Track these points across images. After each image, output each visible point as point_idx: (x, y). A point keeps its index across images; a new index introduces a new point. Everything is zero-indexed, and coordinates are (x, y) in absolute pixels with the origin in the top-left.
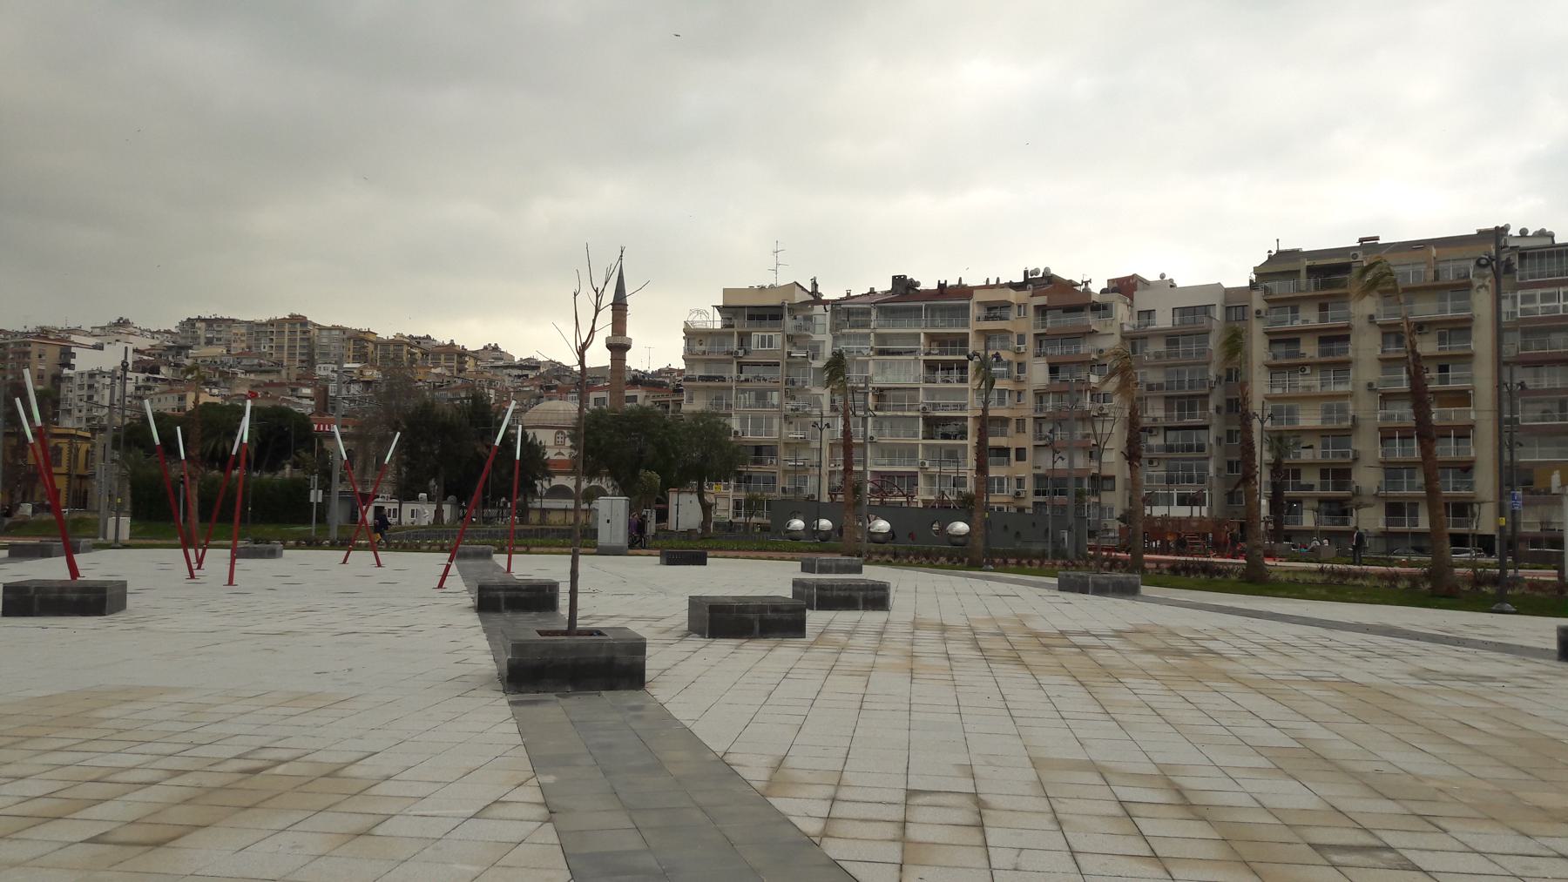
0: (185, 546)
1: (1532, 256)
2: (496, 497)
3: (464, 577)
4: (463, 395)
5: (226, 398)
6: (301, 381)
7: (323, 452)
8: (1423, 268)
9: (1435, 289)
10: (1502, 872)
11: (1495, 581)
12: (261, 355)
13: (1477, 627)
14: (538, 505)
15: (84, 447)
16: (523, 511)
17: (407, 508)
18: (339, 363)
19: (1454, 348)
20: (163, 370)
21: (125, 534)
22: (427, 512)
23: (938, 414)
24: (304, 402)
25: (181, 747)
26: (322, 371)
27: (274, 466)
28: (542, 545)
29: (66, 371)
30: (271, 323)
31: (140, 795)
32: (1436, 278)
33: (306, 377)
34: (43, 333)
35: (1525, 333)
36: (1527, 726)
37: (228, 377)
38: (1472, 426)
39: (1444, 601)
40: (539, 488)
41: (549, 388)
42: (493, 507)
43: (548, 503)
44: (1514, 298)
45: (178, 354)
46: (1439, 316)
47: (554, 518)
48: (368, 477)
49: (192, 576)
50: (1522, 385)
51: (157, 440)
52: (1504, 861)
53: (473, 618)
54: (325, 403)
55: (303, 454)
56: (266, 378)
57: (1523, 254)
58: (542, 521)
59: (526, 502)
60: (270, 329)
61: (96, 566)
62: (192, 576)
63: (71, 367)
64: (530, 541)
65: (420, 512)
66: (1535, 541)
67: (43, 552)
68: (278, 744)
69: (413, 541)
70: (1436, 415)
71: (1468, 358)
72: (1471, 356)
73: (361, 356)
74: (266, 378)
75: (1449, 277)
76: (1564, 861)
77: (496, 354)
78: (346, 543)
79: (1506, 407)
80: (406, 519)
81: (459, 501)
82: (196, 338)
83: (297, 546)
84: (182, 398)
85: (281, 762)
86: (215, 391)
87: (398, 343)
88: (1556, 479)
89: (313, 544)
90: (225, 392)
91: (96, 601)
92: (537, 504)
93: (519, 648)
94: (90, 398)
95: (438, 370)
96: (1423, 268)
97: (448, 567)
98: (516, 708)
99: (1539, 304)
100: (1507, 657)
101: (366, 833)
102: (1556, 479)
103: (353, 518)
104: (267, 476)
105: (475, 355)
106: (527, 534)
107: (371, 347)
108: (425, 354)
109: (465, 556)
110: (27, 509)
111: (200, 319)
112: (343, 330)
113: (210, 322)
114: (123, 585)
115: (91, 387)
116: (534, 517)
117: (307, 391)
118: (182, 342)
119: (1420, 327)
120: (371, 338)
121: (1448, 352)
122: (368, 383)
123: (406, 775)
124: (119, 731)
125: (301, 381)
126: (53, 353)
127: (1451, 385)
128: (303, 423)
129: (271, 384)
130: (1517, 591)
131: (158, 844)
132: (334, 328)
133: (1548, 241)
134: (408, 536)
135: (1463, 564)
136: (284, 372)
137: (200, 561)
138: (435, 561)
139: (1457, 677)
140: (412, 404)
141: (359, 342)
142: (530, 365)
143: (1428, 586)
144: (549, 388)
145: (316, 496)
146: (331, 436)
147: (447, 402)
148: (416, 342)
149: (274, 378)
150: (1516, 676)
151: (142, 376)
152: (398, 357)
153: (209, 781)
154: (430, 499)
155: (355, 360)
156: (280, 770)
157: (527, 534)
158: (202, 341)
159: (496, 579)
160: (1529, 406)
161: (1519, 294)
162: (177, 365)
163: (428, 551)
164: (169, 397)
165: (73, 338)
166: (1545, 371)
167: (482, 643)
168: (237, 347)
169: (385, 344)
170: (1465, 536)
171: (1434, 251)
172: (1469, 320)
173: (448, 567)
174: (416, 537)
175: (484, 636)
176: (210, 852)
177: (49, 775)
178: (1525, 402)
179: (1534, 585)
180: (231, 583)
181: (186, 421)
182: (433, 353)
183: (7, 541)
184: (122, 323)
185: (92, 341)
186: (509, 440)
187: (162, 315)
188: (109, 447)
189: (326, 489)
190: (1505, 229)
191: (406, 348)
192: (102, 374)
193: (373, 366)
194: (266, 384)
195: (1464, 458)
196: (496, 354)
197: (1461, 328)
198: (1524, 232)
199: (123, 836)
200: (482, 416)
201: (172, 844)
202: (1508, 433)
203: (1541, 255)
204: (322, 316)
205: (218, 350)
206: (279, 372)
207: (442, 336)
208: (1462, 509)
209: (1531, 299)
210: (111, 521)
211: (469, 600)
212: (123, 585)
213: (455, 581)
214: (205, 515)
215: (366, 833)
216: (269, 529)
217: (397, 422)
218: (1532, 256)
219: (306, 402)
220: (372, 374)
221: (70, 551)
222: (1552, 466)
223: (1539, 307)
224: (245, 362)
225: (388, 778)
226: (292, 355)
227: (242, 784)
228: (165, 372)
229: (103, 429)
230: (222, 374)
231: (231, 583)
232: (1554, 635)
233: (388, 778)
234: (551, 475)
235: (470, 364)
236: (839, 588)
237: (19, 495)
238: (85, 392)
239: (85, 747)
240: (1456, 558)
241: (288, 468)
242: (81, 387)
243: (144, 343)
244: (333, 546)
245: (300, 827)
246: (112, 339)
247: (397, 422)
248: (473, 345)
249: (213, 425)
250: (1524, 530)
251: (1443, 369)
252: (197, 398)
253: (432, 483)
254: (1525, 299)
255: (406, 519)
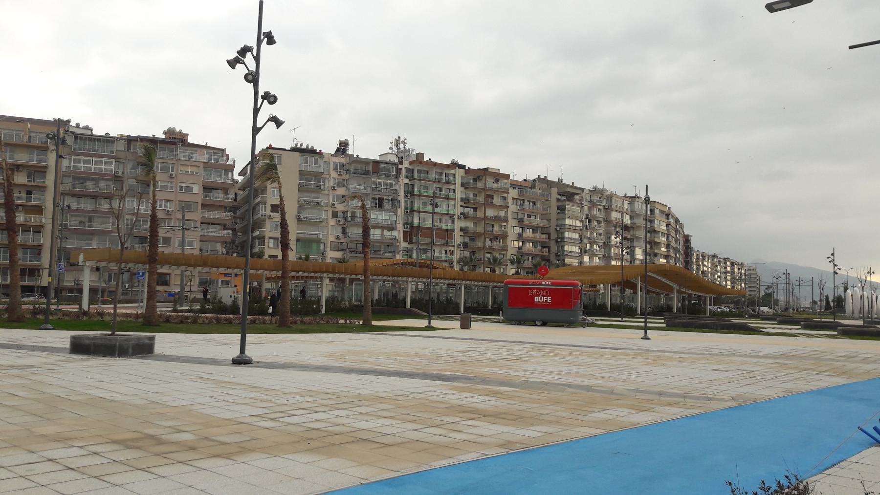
1: (81, 139)
8: (22, 134)
9: (28, 147)
10: (15, 476)
11: (41, 311)
13: (28, 338)
19: (36, 182)
23: (211, 234)
32: (29, 141)
35: (74, 178)
36: (47, 391)
38: (43, 227)
39: (15, 324)
44: (70, 159)
46: (29, 163)
50: (69, 206)
52: (17, 469)
57: (77, 137)
66: (71, 290)
70: (20, 218)
71: (43, 188)
72: (45, 187)
75: (36, 141)
76: (3, 465)
79: (59, 216)
88: (81, 258)
96: (22, 134)
99: (82, 164)
100: (44, 354)
102: (81, 258)
119: (18, 167)
121: (32, 184)
127: (33, 203)
130: (55, 317)
133: (89, 132)
135: (27, 303)
139: (12, 367)
143: (6, 316)
150: (46, 364)
160: (73, 218)
161: (73, 157)
166: (82, 200)
170: (33, 287)
171: (29, 125)
172: (46, 167)
178: (72, 216)
179: (66, 314)
190: (68, 121)
195: (36, 243)
197: (41, 171)
198: (78, 125)
202: (62, 232)
203: (85, 139)
208: (34, 272)
209: (79, 161)
218: (81, 139)
222: (80, 250)
223: (82, 166)
232: (69, 340)
236: (101, 339)
240: (26, 299)
250: (65, 284)
251: (29, 193)
254: (76, 161)
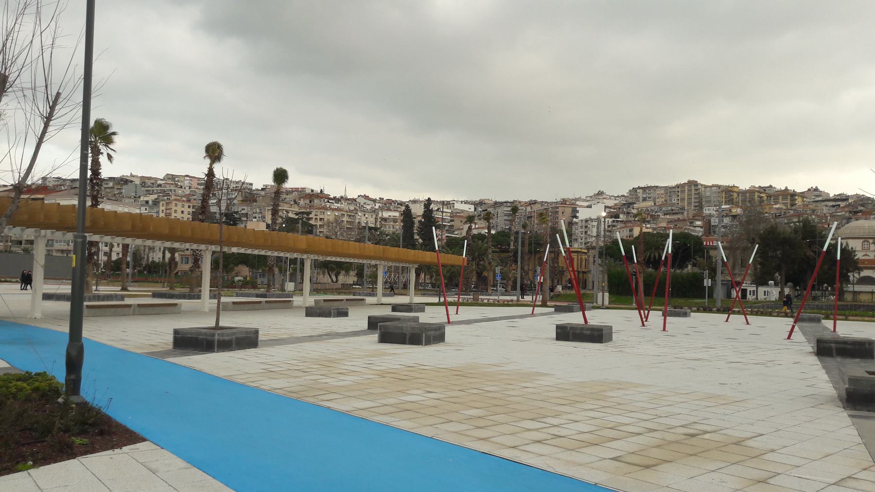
0: (639, 308)
2: (821, 283)
3: (804, 333)
4: (795, 220)
5: (654, 229)
6: (695, 217)
7: (710, 257)
12: (673, 205)
14: (851, 289)
15: (584, 257)
16: (841, 294)
17: (761, 290)
18: (720, 206)
20: (621, 216)
21: (606, 302)
22: (774, 293)
24: (697, 229)
25: (652, 417)
26: (708, 210)
27: (682, 266)
28: (856, 315)
29: (575, 220)
30: (678, 186)
31: (635, 439)
33: (698, 215)
34: (564, 202)
37: (655, 218)
40: (851, 278)
41: (856, 212)
42: (819, 290)
43: (858, 288)
45: (629, 207)
47: (864, 298)
48: (737, 272)
49: (643, 325)
51: (839, 258)
53: (814, 359)
54: (709, 229)
55: (698, 259)
56: (675, 217)
58: (854, 300)
59: (842, 288)
60: (677, 190)
61: (596, 318)
62: (643, 325)
63: (576, 217)
64: (847, 312)
65: (772, 293)
67: (569, 310)
68: (704, 422)
69: (765, 310)
73: (730, 201)
74: (675, 217)
77: (816, 193)
78: (727, 310)
80: (761, 296)
81: (795, 286)
82: (637, 198)
83: (698, 311)
84: (631, 230)
85: (706, 432)
86: (648, 226)
87: (752, 191)
89: (707, 310)
90: (654, 226)
91: (598, 335)
92: (850, 288)
93: (853, 380)
94: (586, 232)
95: (778, 206)
97: (793, 327)
98: (855, 420)
101: (764, 481)
103: (729, 295)
104: (678, 271)
105: (802, 195)
106: (845, 308)
107: (735, 195)
108: (769, 196)
109: (803, 320)
110: (559, 288)
111: (639, 188)
112: (719, 187)
113: (644, 189)
114: (611, 328)
115: (586, 227)
116: (849, 297)
117: (699, 223)
118: (630, 201)
120: (736, 190)
122: (734, 217)
123: (783, 451)
124: (619, 404)
125: (695, 217)
126: (568, 211)
128: (698, 241)
129: (679, 220)
131: (647, 467)
132: (713, 186)
134: (763, 307)
136: (685, 213)
137: (647, 318)
138: (786, 323)
140: (762, 228)
141: (729, 193)
142: (842, 198)
144: (856, 212)
145: (707, 282)
146: (716, 248)
147: (788, 225)
148: (763, 190)
149: (680, 216)
151: (611, 220)
152: (752, 200)
153: (670, 437)
154: (776, 285)
155: (726, 203)
156: (707, 436)
157: (845, 308)
158: (641, 199)
159: (828, 336)
162: (628, 213)
163: (777, 316)
164: (625, 230)
165: (578, 203)
167: (823, 375)
168: (659, 201)
169: (744, 193)
173: (793, 327)
174: (768, 308)
175: (824, 371)
176: (672, 475)
177: (589, 422)
180: (664, 329)
181: (636, 241)
182: (774, 196)
183: (553, 304)
184: (600, 193)
185: (586, 204)
186: (833, 247)
187: (619, 187)
188: (597, 256)
189: (713, 276)
191: (757, 194)
192: (592, 220)
193: (738, 206)
194: (675, 221)
196: (816, 193)
199: (629, 459)
200: (811, 234)
201: (654, 468)
204: (706, 179)
205: (650, 203)
206: (682, 213)
207: (780, 184)
210: (600, 295)
211: (810, 348)
212: (611, 328)
213: (798, 335)
214: (647, 293)
215: (764, 481)
216: (681, 301)
217: (753, 239)
219: (698, 229)
220: (738, 211)
221: (583, 309)
224: (664, 209)
225: (773, 451)
226: (689, 203)
227: (687, 442)
228: (622, 217)
229: (594, 248)
230: (652, 216)
231: (664, 329)
233: (773, 451)
234: (860, 269)
235: (799, 201)
237: (556, 281)
238: (583, 230)
239: (603, 410)
241: (690, 267)
242: (582, 227)
243: (611, 203)
244: (719, 311)
245: (723, 471)
246: (595, 202)
247: (753, 239)
248: (800, 188)
249: (650, 244)
252: (470, 228)
253: (777, 275)
255: (761, 296)
